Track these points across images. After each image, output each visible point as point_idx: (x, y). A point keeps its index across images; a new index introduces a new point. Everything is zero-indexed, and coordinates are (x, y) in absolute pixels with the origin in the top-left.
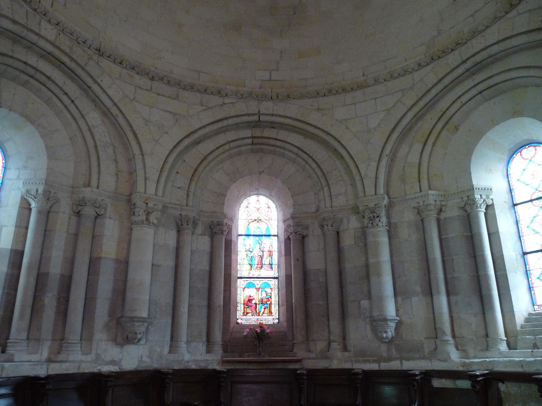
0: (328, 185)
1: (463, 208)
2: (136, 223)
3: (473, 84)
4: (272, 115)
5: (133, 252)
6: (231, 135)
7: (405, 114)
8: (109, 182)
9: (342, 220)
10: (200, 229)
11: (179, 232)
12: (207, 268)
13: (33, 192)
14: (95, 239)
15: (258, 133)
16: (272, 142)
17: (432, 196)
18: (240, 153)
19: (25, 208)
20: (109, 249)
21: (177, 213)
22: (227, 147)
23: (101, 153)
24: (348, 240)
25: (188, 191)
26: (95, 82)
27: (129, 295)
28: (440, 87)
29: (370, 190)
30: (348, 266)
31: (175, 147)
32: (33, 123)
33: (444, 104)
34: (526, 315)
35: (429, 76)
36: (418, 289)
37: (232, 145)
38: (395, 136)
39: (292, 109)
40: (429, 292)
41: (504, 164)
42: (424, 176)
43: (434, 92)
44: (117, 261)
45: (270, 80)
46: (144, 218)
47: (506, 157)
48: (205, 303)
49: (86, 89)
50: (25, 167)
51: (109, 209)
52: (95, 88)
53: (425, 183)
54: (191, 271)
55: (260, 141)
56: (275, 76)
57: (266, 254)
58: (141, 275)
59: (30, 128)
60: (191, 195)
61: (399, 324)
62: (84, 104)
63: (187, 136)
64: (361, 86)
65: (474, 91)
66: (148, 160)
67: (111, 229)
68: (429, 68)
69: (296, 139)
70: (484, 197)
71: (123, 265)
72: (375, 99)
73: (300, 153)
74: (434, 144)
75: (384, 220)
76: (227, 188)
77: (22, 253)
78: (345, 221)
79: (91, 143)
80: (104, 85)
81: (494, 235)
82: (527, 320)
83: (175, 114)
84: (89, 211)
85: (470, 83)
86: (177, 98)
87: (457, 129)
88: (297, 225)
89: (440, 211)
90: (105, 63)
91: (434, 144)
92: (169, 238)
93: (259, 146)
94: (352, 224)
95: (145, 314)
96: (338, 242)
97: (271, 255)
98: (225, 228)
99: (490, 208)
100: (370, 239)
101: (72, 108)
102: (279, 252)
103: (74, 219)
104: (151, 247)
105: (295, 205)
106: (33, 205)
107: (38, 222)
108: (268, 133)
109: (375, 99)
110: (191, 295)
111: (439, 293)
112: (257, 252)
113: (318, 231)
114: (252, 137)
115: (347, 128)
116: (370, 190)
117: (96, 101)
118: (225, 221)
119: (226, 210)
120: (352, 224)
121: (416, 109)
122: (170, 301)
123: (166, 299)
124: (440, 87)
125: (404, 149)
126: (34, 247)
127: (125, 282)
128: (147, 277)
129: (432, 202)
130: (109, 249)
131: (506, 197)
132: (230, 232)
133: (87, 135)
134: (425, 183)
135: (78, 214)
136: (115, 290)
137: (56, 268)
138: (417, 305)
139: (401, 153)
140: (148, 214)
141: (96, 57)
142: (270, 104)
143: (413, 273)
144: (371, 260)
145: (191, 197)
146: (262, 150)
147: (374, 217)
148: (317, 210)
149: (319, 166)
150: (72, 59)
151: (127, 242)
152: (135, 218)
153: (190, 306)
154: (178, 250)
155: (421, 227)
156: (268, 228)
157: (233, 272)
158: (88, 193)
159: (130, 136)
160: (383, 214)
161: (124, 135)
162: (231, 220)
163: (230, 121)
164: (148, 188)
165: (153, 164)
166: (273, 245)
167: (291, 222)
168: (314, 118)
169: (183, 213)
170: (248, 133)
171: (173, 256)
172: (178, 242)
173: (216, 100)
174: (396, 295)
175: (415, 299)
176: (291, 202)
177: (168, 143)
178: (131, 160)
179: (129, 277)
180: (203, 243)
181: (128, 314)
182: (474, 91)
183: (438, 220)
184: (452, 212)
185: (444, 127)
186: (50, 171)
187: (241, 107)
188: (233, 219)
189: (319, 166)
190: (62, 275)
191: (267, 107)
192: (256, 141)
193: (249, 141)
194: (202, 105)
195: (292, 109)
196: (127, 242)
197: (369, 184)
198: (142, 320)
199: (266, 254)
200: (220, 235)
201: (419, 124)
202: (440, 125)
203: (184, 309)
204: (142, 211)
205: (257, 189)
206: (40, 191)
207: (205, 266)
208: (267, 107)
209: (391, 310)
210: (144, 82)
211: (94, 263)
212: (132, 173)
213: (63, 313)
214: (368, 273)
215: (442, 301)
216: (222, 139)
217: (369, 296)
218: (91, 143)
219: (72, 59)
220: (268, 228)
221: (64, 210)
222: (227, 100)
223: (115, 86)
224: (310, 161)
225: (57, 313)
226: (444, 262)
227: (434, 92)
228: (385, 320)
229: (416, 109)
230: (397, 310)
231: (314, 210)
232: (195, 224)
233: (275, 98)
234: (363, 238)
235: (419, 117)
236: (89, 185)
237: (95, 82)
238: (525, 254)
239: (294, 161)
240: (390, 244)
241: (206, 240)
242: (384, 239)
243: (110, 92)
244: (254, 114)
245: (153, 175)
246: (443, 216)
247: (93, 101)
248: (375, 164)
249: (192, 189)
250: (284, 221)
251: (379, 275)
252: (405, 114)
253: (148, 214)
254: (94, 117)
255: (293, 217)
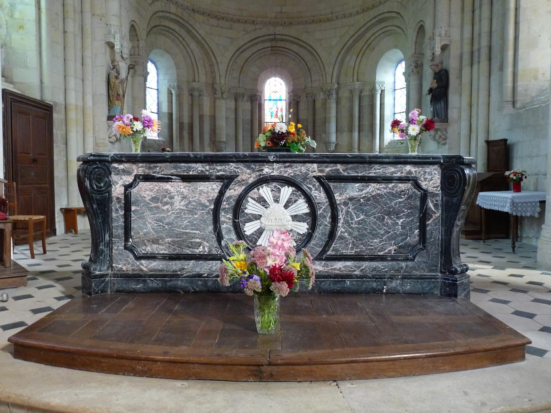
0: (311, 75)
1: (371, 91)
2: (218, 99)
3: (380, 28)
4: (282, 35)
5: (217, 112)
6: (260, 46)
7: (349, 40)
8: (203, 78)
9: (316, 95)
10: (246, 98)
11: (236, 100)
12: (250, 118)
13: (172, 86)
14: (200, 106)
15: (274, 44)
16: (282, 49)
17: (357, 84)
18: (265, 55)
19: (170, 94)
20: (207, 111)
21: (235, 91)
22: (258, 53)
23: (198, 64)
24: (318, 105)
25: (239, 79)
26: (194, 28)
27: (217, 131)
28: (365, 28)
29: (329, 81)
30: (317, 117)
31: (232, 57)
32: (168, 53)
33: (368, 35)
34: (389, 141)
35: (361, 19)
36: (346, 129)
37: (260, 51)
38: (343, 51)
39: (293, 31)
40: (351, 131)
41: (394, 68)
42: (355, 74)
43: (363, 30)
44: (210, 116)
45: (281, 12)
46: (221, 96)
47: (395, 65)
48: (250, 135)
49: (189, 32)
50: (166, 74)
51: (204, 92)
52: (193, 31)
53: (355, 77)
54: (243, 120)
55: (276, 49)
56: (284, 9)
57: (279, 110)
58: (222, 123)
59: (167, 55)
60: (241, 81)
61: (337, 145)
62: (189, 39)
63: (237, 50)
64: (329, 20)
65: (380, 32)
66: (220, 66)
67: (206, 102)
68: (362, 15)
69: (295, 48)
70: (381, 86)
71: (213, 118)
72: (336, 28)
73: (297, 55)
74: (362, 57)
75: (334, 96)
76: (259, 75)
77: (172, 114)
78: (318, 95)
79: (193, 59)
80: (197, 28)
81: (382, 105)
82: (389, 143)
83: (231, 38)
84: (196, 94)
85: (379, 27)
86: (231, 29)
87: (374, 49)
88: (295, 95)
89: (361, 92)
90: (197, 16)
91: (362, 57)
92: (232, 104)
93: (275, 50)
94: (322, 96)
95: (224, 140)
96: (314, 105)
97: (282, 110)
98: (258, 98)
99: (383, 91)
100: (327, 105)
101: (184, 43)
102: (286, 109)
103: (190, 97)
104: (225, 107)
105: (294, 85)
106: (173, 92)
107: (176, 100)
108: (280, 44)
109: (336, 28)
110: (243, 132)
111: (355, 131)
112: (274, 110)
113: (305, 99)
114: (271, 47)
115: (321, 45)
116: (329, 81)
117: (193, 37)
118: (258, 94)
119: (258, 88)
120: (321, 96)
121: (354, 38)
122: (234, 134)
123: (232, 133)
124: (365, 28)
125: (348, 58)
126: (176, 111)
127: (215, 125)
128: (224, 124)
129: (357, 87)
130: (207, 111)
131: (391, 86)
132: (261, 98)
133: (191, 55)
134: (355, 77)
135: (191, 95)
136: (211, 130)
137: (186, 120)
138: (345, 136)
139: (347, 60)
140: (222, 94)
141: (192, 15)
142: (281, 28)
143: (345, 123)
144: (327, 116)
145: (241, 83)
146: (277, 53)
147: (328, 94)
148: (305, 88)
149: (306, 64)
150: (183, 19)
151: (214, 107)
152: (216, 96)
153: (243, 136)
154: (236, 110)
155: (351, 100)
156: (280, 96)
157: (262, 120)
158: (195, 85)
159: (211, 54)
160: (334, 93)
161: (208, 53)
162: (261, 93)
163: (260, 39)
164: (222, 81)
165: (223, 67)
166: (283, 105)
167: (291, 94)
168: (304, 37)
169: (238, 91)
170: (269, 44)
171: (233, 113)
172: (236, 105)
173: (251, 27)
174: (337, 132)
175: (345, 134)
176: (292, 83)
177: (229, 55)
178: (212, 65)
179: (217, 123)
180: (248, 106)
181: (217, 140)
182: (380, 32)
183: (360, 96)
184: (366, 93)
185: (367, 48)
186: (178, 75)
187: (265, 31)
188: (262, 92)
189: (306, 64)
190: (189, 123)
191: (279, 30)
192: (273, 49)
193: (270, 49)
194: (244, 31)
195: (293, 31)
196: (214, 107)
197: (329, 77)
198: (225, 142)
199: (279, 110)
200: (256, 101)
201: (356, 45)
202: (365, 47)
203: (240, 137)
204: (219, 93)
205: (275, 75)
206: (175, 85)
207: (249, 117)
208: (279, 30)
209: (333, 138)
210: (214, 22)
211: (201, 117)
212: (213, 72)
213: (191, 139)
214: (325, 121)
215: (356, 134)
216: (255, 49)
217: (325, 132)
218: (193, 59)
219: (183, 19)
220: (280, 96)
221: (186, 92)
222: (257, 27)
223: (202, 27)
224: (302, 61)
225: (189, 139)
226: (359, 117)
227: (363, 30)
228: (330, 143)
229: (354, 38)
230: (337, 138)
231: (303, 88)
232: (243, 96)
233: (284, 24)
234: (325, 103)
235: (356, 41)
236: (194, 81)
237: (194, 28)
238: (395, 114)
239: (294, 60)
240: (337, 108)
241: (249, 104)
242: (334, 106)
243: (200, 32)
244: (273, 35)
245: (223, 73)
246: (362, 94)
247: (192, 36)
248: (333, 66)
249: (241, 78)
250: (288, 93)
251: (329, 123)
252: (349, 40)
253: (222, 94)
254: (193, 45)
255: (293, 92)
